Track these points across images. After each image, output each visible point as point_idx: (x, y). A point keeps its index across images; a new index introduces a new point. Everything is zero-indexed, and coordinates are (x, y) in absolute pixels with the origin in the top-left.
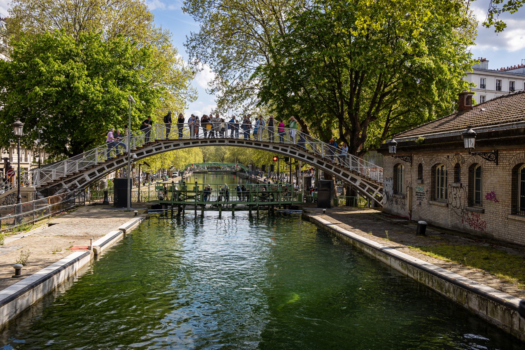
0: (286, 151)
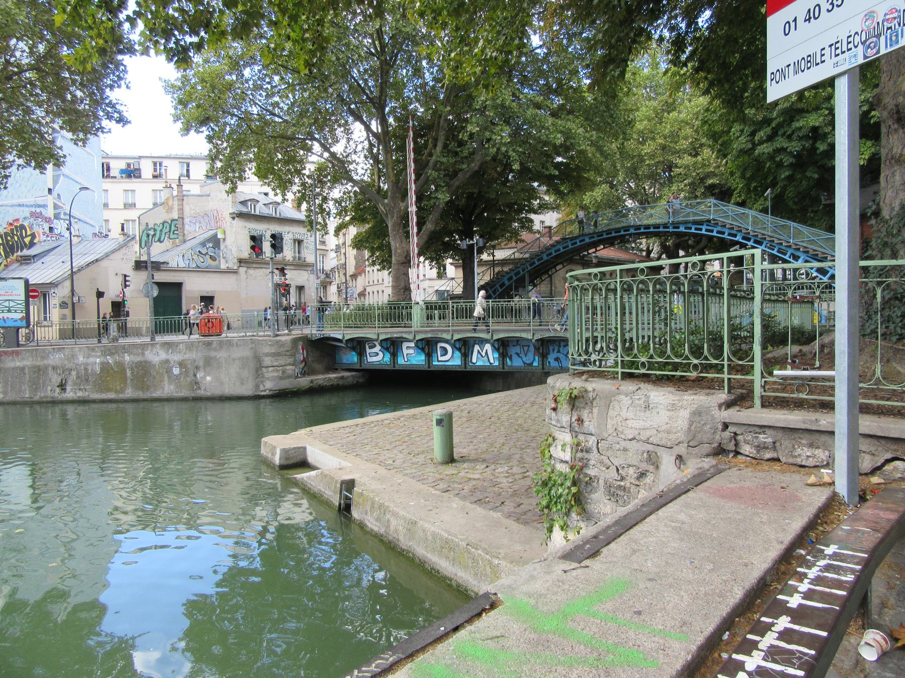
0: (701, 230)
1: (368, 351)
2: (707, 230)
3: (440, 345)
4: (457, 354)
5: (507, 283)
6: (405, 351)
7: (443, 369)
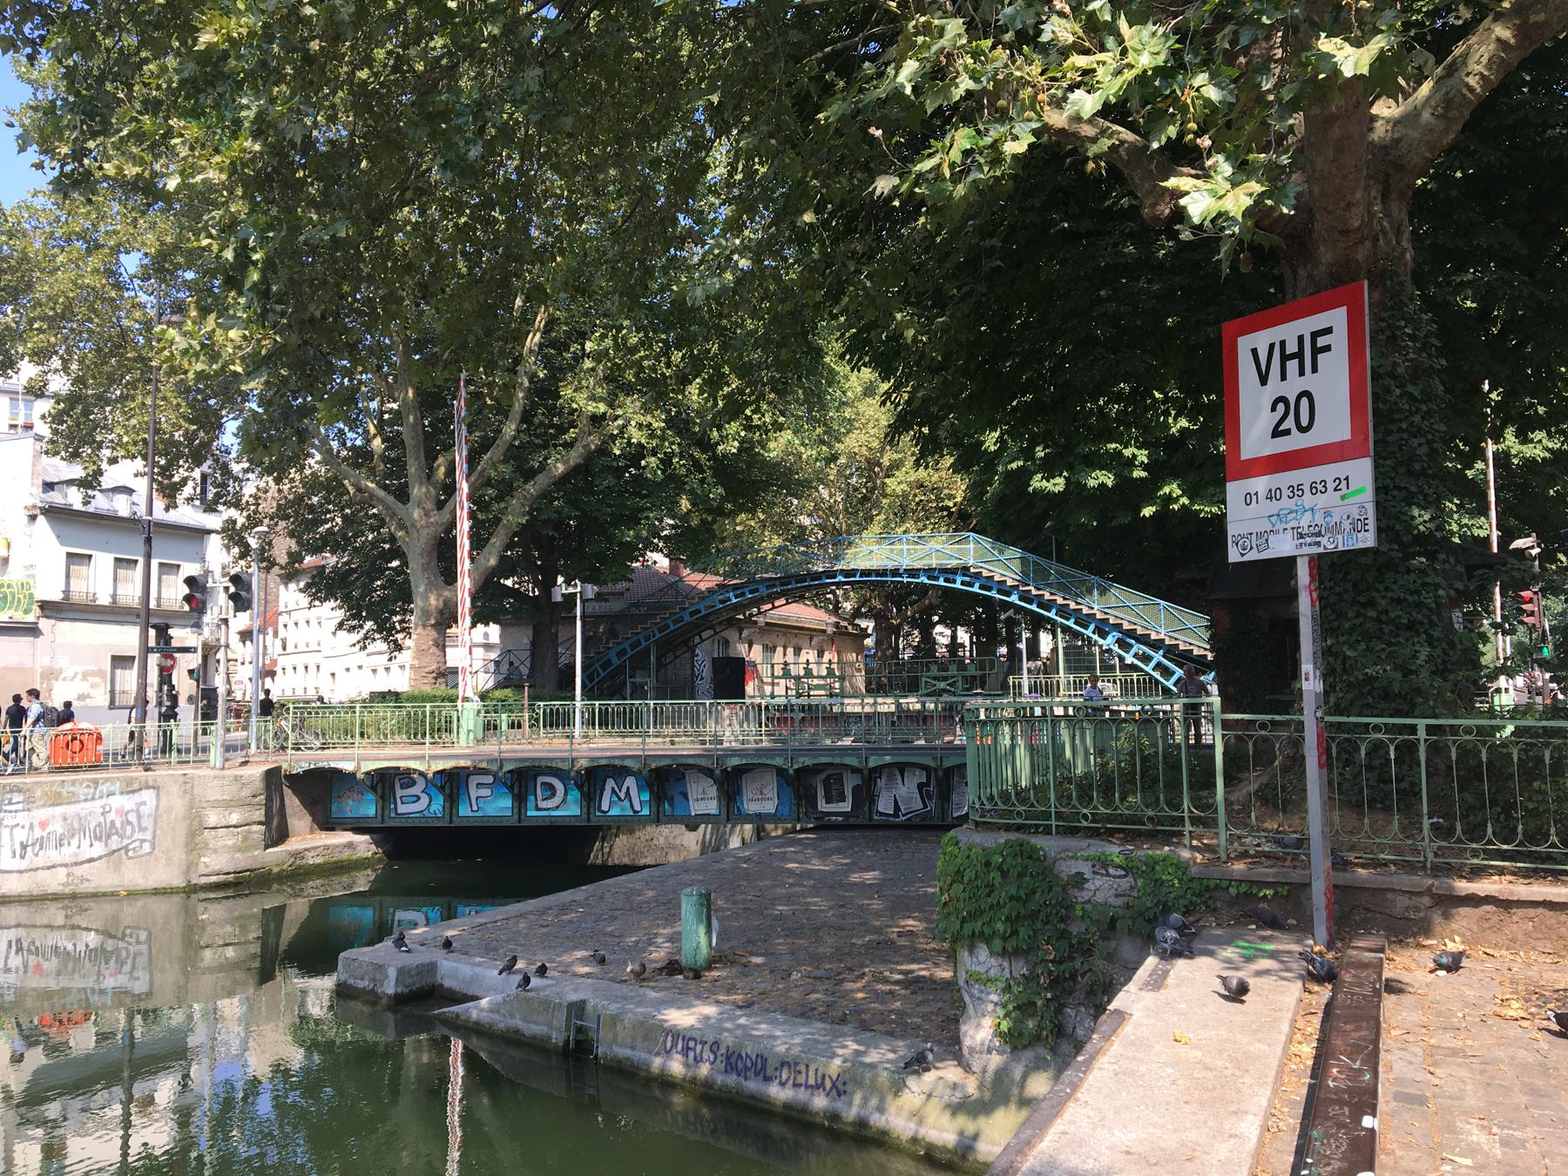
1: (399, 792)
2: (963, 583)
3: (541, 779)
4: (575, 794)
5: (616, 661)
6: (474, 792)
7: (548, 822)
